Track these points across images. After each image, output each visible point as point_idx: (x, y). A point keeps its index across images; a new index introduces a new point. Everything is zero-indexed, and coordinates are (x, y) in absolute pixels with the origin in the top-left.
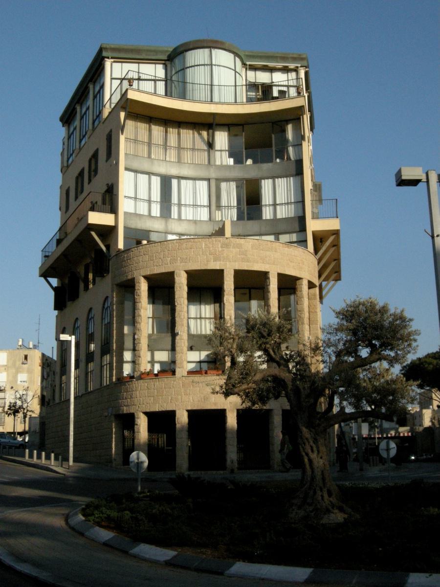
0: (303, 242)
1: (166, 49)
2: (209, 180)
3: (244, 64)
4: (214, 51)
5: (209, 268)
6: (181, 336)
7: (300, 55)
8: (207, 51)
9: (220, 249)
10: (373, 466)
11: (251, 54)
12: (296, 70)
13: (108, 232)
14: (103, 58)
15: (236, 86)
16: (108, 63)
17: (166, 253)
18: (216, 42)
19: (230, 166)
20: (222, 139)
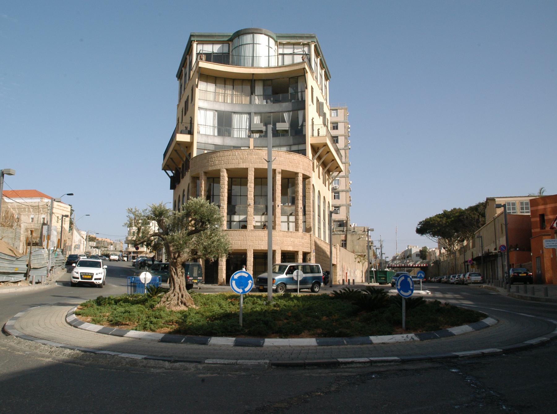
0: (303, 152)
1: (229, 34)
2: (249, 114)
3: (276, 42)
4: (256, 35)
5: (239, 167)
6: (223, 206)
7: (311, 35)
8: (252, 35)
9: (246, 156)
10: (267, 286)
11: (281, 35)
12: (308, 45)
13: (189, 146)
14: (192, 41)
15: (269, 56)
16: (195, 45)
17: (216, 158)
18: (257, 29)
19: (265, 105)
20: (259, 89)
